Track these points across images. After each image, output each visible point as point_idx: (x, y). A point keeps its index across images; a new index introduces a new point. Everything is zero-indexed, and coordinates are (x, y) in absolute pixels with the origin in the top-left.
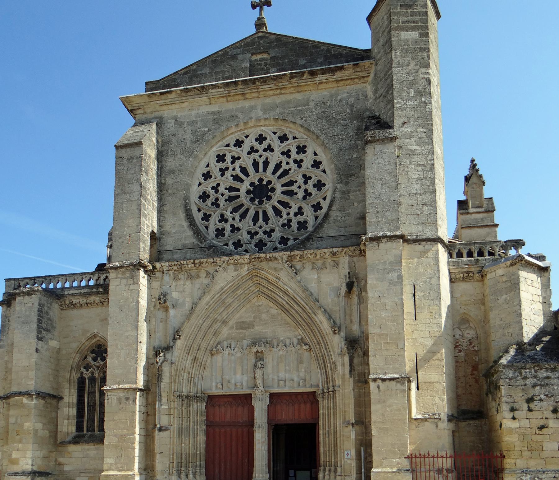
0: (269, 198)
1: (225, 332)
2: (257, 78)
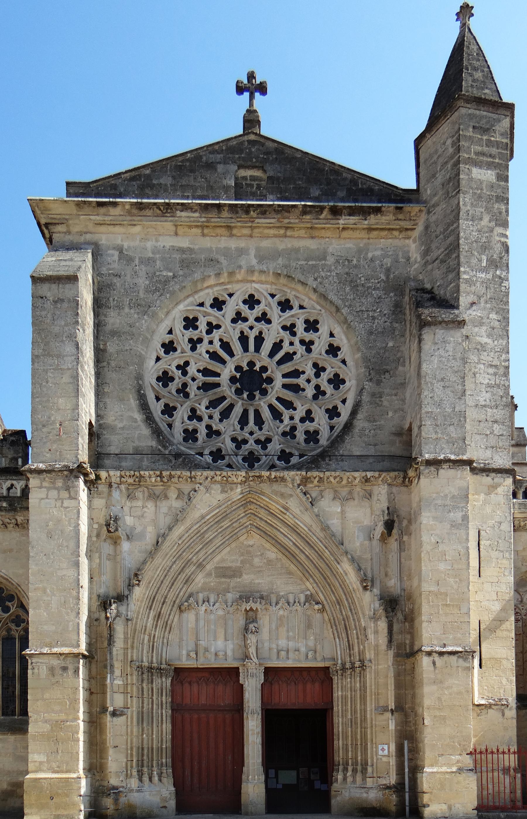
0: (264, 392)
1: (200, 579)
2: (253, 205)
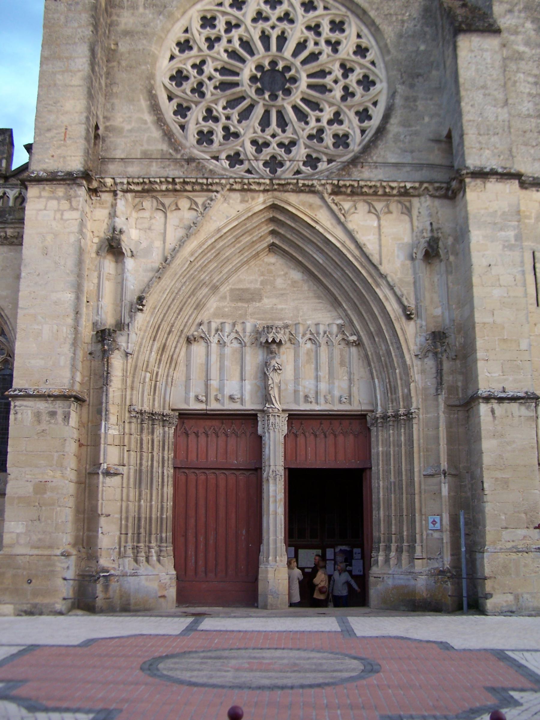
0: (288, 92)
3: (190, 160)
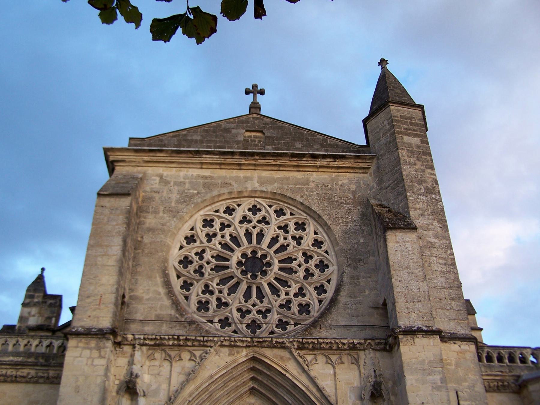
0: (264, 273)
3: (191, 323)
